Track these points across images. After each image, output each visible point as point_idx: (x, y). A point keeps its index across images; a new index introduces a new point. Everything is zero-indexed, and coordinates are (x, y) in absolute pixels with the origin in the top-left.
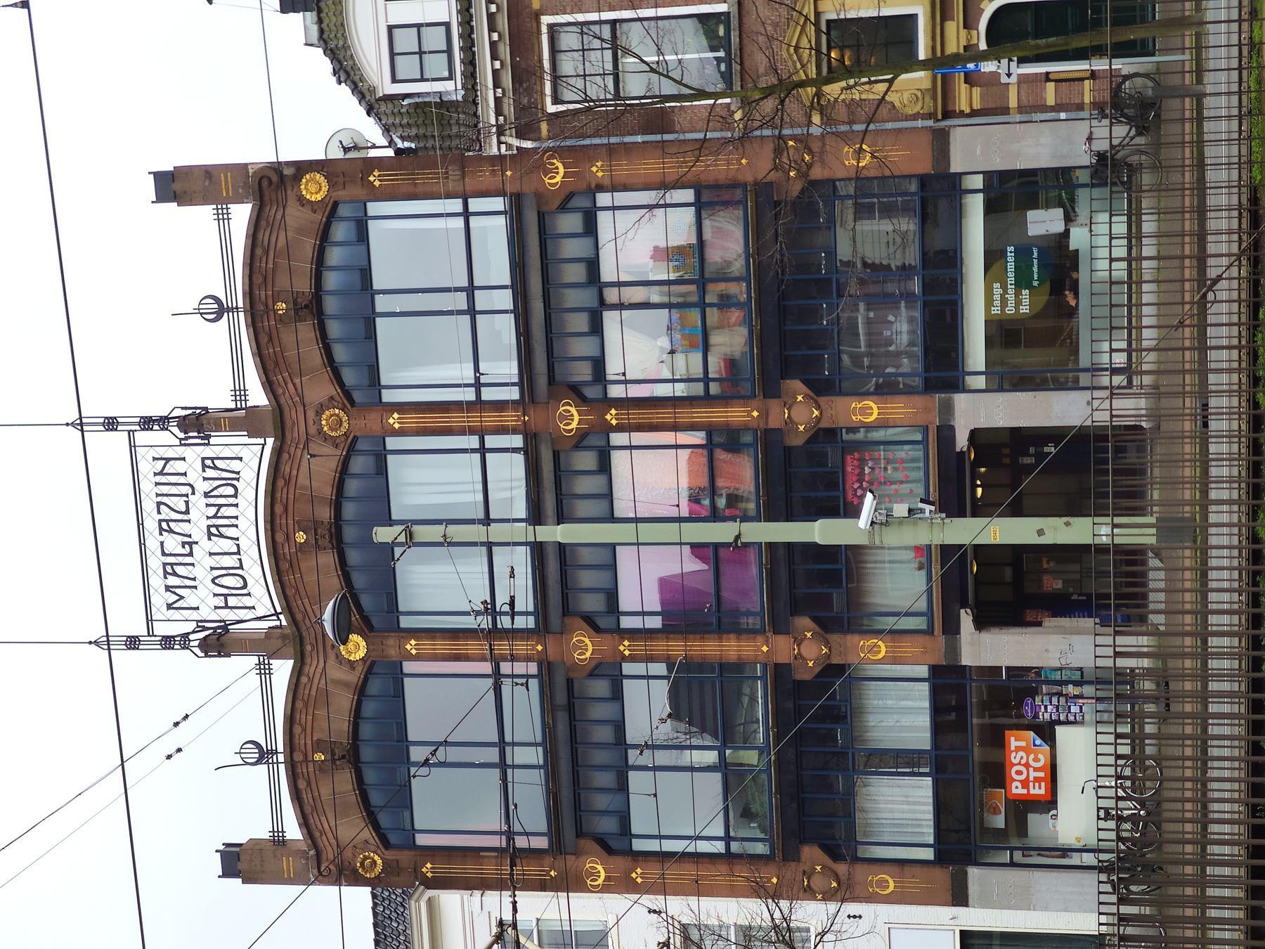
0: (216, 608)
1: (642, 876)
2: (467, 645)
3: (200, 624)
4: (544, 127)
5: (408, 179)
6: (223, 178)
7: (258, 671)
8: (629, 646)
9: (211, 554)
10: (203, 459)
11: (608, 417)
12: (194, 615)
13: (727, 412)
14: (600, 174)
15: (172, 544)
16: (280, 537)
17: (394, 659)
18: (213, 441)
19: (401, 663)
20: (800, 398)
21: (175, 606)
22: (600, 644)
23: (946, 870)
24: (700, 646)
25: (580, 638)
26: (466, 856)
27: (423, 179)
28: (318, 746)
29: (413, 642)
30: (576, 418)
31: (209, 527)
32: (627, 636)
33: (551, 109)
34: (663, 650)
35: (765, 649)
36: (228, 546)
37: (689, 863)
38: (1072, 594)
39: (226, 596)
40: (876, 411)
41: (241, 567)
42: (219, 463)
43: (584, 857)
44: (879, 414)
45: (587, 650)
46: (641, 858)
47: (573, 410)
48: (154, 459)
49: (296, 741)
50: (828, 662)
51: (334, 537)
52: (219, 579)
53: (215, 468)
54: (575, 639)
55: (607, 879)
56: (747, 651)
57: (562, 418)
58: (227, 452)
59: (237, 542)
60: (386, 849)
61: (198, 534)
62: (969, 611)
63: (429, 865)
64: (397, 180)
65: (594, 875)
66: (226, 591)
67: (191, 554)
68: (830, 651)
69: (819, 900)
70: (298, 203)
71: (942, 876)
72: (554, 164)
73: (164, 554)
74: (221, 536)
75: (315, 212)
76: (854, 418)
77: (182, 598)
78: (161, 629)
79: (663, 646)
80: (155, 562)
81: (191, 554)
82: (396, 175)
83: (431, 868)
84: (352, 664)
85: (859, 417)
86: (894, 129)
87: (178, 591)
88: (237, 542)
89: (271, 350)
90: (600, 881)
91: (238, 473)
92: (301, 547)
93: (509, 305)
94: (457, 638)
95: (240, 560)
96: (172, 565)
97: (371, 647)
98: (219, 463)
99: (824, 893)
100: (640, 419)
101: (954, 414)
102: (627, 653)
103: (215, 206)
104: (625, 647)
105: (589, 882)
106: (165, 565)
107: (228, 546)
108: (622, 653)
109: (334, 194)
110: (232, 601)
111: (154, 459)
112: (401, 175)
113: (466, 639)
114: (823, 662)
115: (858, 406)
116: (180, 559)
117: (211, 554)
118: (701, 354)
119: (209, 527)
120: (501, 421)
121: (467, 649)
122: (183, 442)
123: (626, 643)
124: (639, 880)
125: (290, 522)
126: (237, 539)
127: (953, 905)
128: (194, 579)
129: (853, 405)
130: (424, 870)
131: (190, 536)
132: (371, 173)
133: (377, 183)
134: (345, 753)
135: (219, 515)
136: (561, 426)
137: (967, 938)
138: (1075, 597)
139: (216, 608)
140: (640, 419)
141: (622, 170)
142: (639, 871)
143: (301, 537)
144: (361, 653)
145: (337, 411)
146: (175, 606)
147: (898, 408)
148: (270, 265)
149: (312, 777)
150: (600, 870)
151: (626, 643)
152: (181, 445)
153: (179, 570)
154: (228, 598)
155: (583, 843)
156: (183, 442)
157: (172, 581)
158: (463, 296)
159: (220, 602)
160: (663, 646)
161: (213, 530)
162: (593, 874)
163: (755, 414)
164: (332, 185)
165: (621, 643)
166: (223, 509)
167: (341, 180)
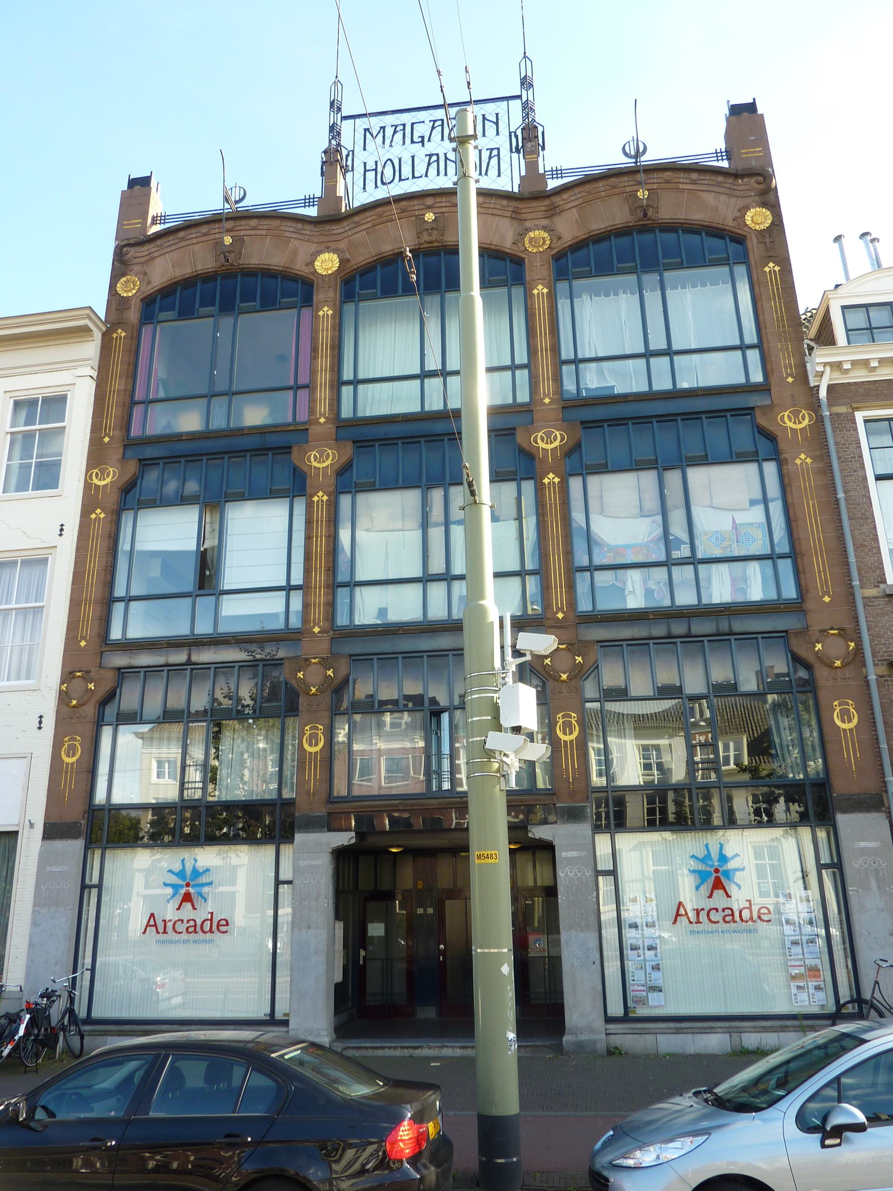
0: (365, 164)
1: (98, 519)
2: (326, 357)
3: (351, 153)
4: (842, 409)
5: (774, 294)
6: (757, 149)
7: (307, 197)
8: (322, 501)
9: (413, 157)
10: (498, 149)
11: (551, 475)
12: (359, 149)
13: (561, 587)
14: (798, 462)
15: (422, 130)
16: (429, 201)
17: (315, 298)
18: (515, 156)
19: (304, 495)
20: (579, 659)
21: (367, 133)
22: (325, 475)
23: (81, 817)
24: (321, 567)
25: (331, 456)
26: (129, 365)
27: (776, 307)
28: (238, 241)
29: (330, 312)
30: (549, 447)
31: (437, 155)
32: (332, 498)
33: (859, 416)
34: (317, 532)
35: (316, 630)
36: (420, 169)
37: (107, 562)
38: (364, 949)
39: (376, 170)
40: (567, 738)
41: (400, 180)
42: (494, 161)
43: (119, 466)
44: (565, 742)
45: (319, 462)
46: (114, 517)
47: (557, 443)
48: (497, 114)
49: (243, 222)
50: (301, 693)
51: (429, 245)
52: (391, 164)
53: (490, 158)
54: (330, 451)
55: (97, 487)
56: (314, 613)
57: (549, 435)
58: (505, 166)
59: (423, 176)
60: (141, 300)
61: (430, 148)
62: (353, 841)
63: (123, 334)
64: (772, 285)
65: (102, 475)
66: (380, 169)
67: (413, 142)
68: (313, 695)
69: (60, 687)
70: (741, 206)
71: (75, 813)
72: (804, 419)
73: (413, 124)
74: (429, 164)
75: (734, 219)
76: (560, 715)
77: (374, 138)
78: (346, 128)
79: (321, 532)
80: (407, 118)
81: (413, 142)
82: (777, 285)
83: (121, 337)
84: (311, 263)
85: (561, 721)
86: (880, 752)
87: (381, 135)
88: (423, 176)
89: (602, 189)
90: (96, 481)
91: (486, 174)
92: (421, 218)
93: (656, 387)
94: (333, 348)
95: (408, 179)
96: (404, 129)
97: (327, 279)
98: (494, 161)
99: (66, 693)
100: (551, 505)
101: (569, 823)
102: (315, 499)
103: (723, 150)
104: (321, 497)
105: (95, 471)
106: (404, 125)
107: (420, 169)
108: (316, 494)
109: (753, 236)
110: (371, 175)
111: (497, 114)
112: (778, 289)
113: (332, 356)
114: (300, 688)
115: (573, 720)
116: (408, 136)
117: (413, 157)
118: (768, 497)
119: (437, 155)
120: (543, 380)
121: (322, 357)
122: (513, 134)
123: (325, 498)
124: (93, 516)
125: (444, 210)
126: (426, 176)
127: (45, 824)
128: (391, 146)
129: (573, 715)
130: (119, 331)
131: (429, 140)
132: (776, 264)
133: (767, 269)
134: (230, 261)
135: (448, 162)
136: (541, 433)
137: (12, 836)
138: (362, 953)
139: (365, 164)
140: (551, 505)
141: (804, 481)
142: (102, 516)
143: (429, 216)
144: (326, 256)
145: (548, 242)
146: (367, 133)
147: (573, 763)
148: (681, 186)
149: (212, 237)
150: (106, 481)
151: (325, 498)
152: (510, 133)
153: (399, 135)
154: (374, 172)
155: (132, 467)
156: (513, 134)
157: (389, 131)
158: (663, 345)
159: (371, 165)
160: (321, 532)
161: (434, 158)
162: (102, 474)
163: (560, 615)
164: (761, 233)
165: (325, 493)
166: (453, 164)
167: (767, 240)
